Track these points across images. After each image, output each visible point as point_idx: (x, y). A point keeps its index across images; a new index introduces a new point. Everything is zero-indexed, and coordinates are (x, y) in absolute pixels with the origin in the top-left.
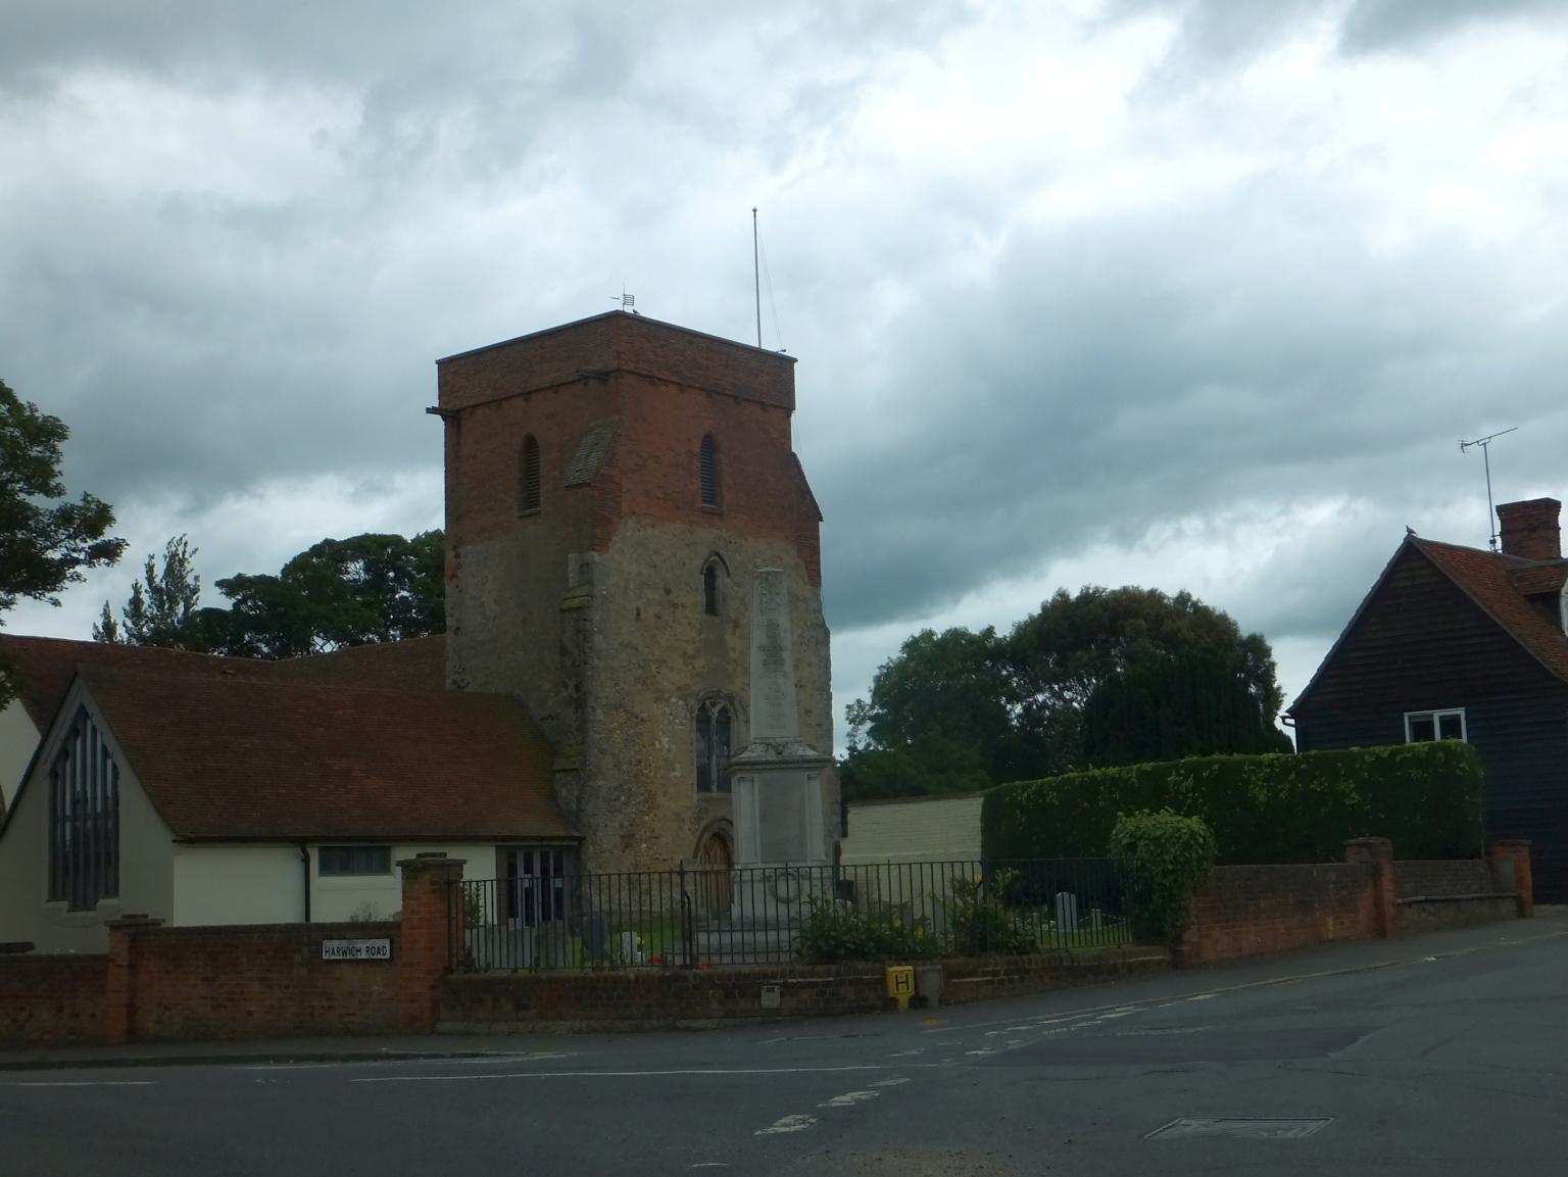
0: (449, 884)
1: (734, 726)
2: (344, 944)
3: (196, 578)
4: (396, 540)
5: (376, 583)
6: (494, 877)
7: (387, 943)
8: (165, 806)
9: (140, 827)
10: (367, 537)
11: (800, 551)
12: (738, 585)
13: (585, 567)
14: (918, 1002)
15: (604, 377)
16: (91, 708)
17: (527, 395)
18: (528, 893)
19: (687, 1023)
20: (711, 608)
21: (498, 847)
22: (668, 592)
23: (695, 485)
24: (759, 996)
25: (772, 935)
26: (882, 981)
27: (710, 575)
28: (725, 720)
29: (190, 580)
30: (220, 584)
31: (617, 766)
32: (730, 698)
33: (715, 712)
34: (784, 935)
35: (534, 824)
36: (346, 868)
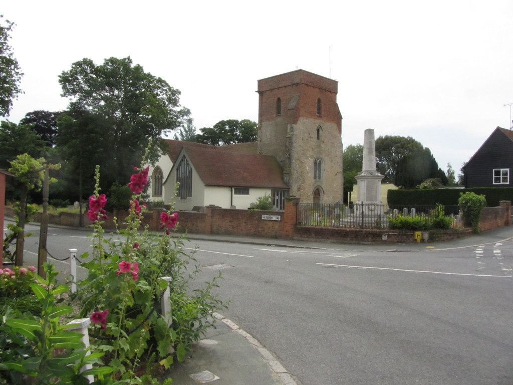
0: (297, 204)
1: (322, 165)
2: (268, 216)
3: (195, 128)
4: (237, 121)
5: (232, 131)
6: (313, 203)
7: (280, 217)
8: (202, 177)
9: (197, 181)
10: (230, 120)
11: (338, 126)
12: (324, 133)
13: (292, 128)
14: (423, 241)
15: (297, 84)
16: (186, 156)
17: (278, 88)
18: (277, 200)
19: (363, 242)
20: (318, 138)
21: (272, 190)
22: (309, 134)
23: (316, 110)
24: (381, 237)
25: (370, 219)
26: (413, 235)
27: (318, 130)
28: (320, 164)
29: (193, 128)
30: (200, 129)
31: (297, 173)
32: (321, 159)
33: (318, 162)
34: (373, 219)
35: (279, 184)
36: (239, 193)
